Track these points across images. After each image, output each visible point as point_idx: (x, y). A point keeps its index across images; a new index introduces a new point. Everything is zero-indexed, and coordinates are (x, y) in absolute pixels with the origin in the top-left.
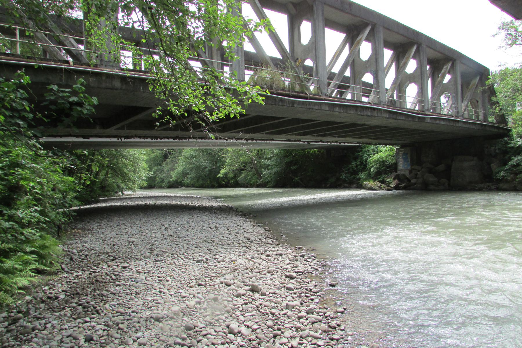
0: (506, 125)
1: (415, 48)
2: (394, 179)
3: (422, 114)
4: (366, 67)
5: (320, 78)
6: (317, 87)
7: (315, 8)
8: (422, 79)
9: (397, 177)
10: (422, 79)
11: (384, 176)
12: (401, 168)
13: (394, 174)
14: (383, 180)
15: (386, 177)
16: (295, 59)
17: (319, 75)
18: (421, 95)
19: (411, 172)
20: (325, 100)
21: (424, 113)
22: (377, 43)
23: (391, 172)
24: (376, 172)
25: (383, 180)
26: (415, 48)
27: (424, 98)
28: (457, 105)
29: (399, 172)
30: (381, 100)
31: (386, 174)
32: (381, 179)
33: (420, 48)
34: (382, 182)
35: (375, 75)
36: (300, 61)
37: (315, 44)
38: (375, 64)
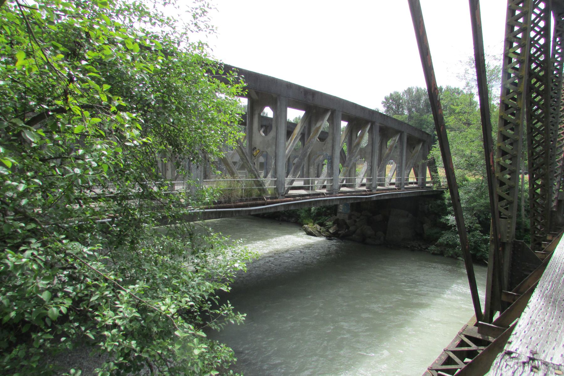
0: (491, 342)
1: (369, 126)
2: (334, 223)
3: (369, 195)
4: (322, 149)
5: (278, 178)
6: (275, 188)
7: (279, 104)
8: (372, 157)
9: (336, 222)
10: (372, 157)
11: (324, 217)
12: (341, 211)
13: (334, 217)
14: (323, 222)
15: (326, 220)
16: (253, 147)
17: (278, 176)
18: (369, 172)
19: (350, 217)
20: (282, 202)
21: (371, 193)
22: (335, 128)
23: (330, 214)
24: (317, 213)
25: (323, 222)
26: (369, 126)
27: (373, 177)
28: (401, 176)
29: (338, 216)
30: (334, 187)
31: (326, 215)
32: (320, 221)
33: (374, 126)
34: (321, 224)
35: (330, 161)
36: (258, 152)
37: (276, 140)
38: (331, 149)
